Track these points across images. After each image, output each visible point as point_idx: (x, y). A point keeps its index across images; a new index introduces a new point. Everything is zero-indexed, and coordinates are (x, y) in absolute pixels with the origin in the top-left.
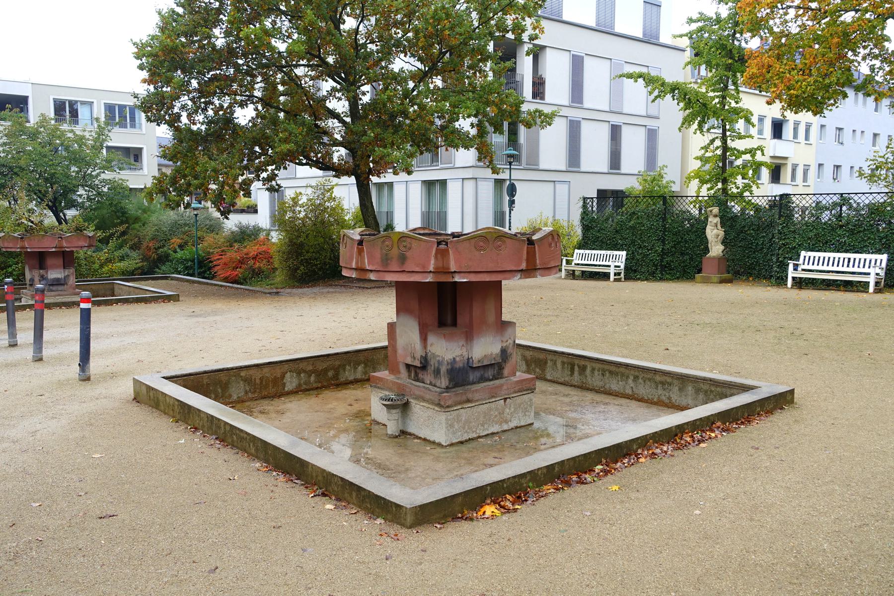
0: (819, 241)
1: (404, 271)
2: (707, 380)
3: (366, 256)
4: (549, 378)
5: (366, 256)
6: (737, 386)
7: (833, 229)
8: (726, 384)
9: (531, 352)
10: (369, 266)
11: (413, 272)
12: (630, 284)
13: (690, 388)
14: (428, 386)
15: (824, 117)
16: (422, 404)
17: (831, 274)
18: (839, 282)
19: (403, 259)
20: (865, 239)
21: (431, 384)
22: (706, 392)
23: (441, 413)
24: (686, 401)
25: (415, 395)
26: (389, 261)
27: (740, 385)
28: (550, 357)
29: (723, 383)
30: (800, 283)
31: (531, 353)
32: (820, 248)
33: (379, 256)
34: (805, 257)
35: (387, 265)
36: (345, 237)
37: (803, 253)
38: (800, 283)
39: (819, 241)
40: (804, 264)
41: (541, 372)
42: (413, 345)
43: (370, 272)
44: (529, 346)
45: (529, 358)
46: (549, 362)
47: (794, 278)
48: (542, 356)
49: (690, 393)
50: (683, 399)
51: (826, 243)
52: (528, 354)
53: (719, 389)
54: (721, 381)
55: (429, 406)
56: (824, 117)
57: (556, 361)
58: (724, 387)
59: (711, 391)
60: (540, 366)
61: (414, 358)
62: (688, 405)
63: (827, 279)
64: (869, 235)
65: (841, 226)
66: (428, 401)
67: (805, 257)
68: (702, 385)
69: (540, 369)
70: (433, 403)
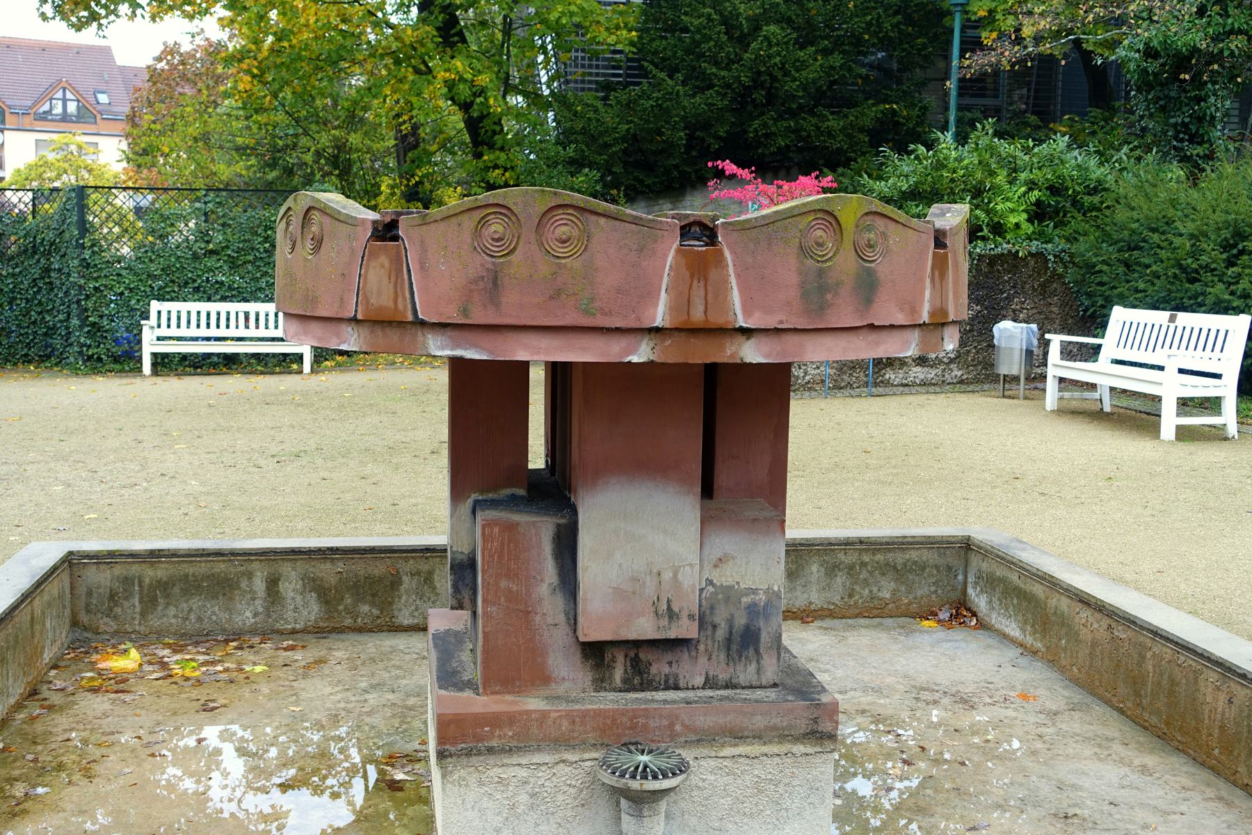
0: (173, 281)
1: (871, 327)
2: (852, 544)
3: (733, 280)
4: (407, 622)
5: (733, 280)
6: (917, 543)
7: (195, 257)
8: (893, 543)
9: (341, 564)
10: (747, 312)
11: (892, 327)
12: (159, 380)
13: (814, 568)
14: (701, 693)
15: (104, 37)
16: (728, 751)
17: (229, 342)
18: (215, 359)
19: (868, 286)
20: (258, 275)
21: (710, 683)
22: (851, 567)
23: (818, 760)
24: (806, 596)
25: (695, 730)
26: (829, 296)
27: (924, 540)
28: (407, 567)
29: (887, 543)
30: (163, 364)
31: (340, 567)
32: (174, 295)
33: (793, 279)
34: (159, 312)
35: (822, 308)
36: (316, 216)
37: (155, 306)
38: (163, 364)
39: (173, 281)
40: (159, 326)
41: (376, 612)
42: (667, 575)
43: (740, 339)
44: (331, 549)
45: (333, 580)
46: (406, 579)
47: (154, 355)
48: (378, 569)
49: (814, 578)
50: (799, 593)
51: (186, 283)
52: (328, 572)
53: (879, 557)
54: (884, 540)
55: (765, 749)
56: (104, 37)
57: (431, 573)
58: (890, 550)
59: (863, 564)
60: (373, 596)
61: (672, 615)
62: (811, 603)
63: (192, 354)
64: (265, 269)
65: (212, 252)
66: (760, 738)
67: (159, 312)
68: (841, 556)
69: (373, 604)
70: (784, 735)
